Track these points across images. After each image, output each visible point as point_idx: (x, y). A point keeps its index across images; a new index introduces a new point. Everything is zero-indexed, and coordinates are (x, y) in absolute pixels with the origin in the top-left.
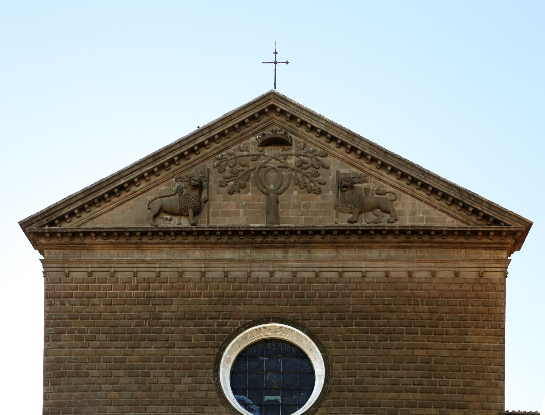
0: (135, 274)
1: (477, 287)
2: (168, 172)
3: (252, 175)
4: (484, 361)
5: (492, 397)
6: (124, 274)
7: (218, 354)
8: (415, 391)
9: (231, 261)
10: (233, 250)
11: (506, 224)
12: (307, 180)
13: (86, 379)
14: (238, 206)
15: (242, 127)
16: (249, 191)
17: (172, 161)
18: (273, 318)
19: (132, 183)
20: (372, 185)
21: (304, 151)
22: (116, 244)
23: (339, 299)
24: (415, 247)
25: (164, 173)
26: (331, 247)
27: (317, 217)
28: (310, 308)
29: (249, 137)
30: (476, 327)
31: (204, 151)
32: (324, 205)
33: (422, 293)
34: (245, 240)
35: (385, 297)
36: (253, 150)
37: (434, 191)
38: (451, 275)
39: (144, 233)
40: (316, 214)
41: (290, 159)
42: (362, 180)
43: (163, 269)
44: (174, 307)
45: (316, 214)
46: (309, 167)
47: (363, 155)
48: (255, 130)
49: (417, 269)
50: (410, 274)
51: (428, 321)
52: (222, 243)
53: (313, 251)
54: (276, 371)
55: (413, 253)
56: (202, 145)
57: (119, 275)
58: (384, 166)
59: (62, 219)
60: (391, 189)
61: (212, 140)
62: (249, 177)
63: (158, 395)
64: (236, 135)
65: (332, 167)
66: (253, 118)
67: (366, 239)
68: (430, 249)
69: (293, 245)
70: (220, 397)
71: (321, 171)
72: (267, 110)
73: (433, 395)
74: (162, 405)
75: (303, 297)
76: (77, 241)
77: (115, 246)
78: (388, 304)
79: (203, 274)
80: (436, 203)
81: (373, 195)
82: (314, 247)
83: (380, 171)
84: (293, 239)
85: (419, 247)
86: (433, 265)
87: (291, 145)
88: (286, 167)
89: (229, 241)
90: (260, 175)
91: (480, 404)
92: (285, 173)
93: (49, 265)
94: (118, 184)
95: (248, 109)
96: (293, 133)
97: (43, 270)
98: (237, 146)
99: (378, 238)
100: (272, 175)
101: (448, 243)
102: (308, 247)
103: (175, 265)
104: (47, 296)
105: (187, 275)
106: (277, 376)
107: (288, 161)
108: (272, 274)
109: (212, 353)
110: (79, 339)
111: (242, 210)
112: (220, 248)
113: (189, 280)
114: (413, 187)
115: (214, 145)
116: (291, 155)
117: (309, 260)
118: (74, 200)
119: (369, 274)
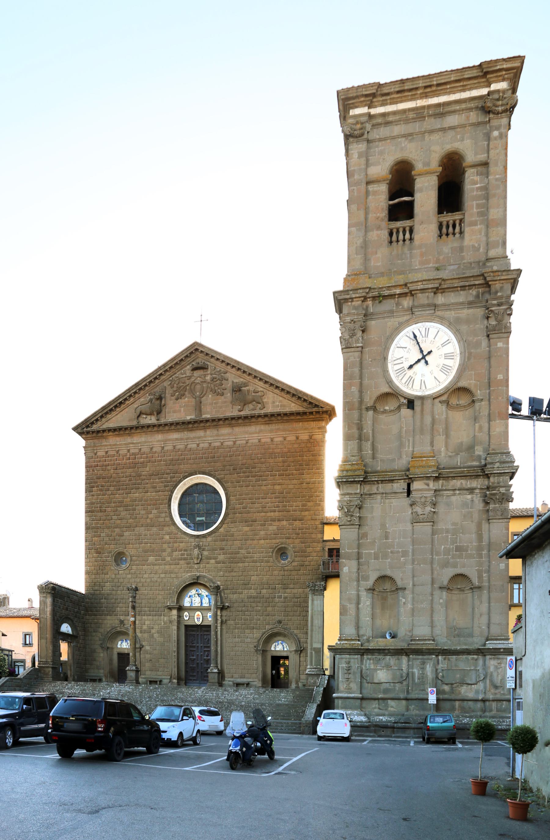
0: (129, 451)
1: (309, 445)
2: (144, 391)
3: (188, 388)
4: (313, 490)
5: (317, 512)
6: (123, 451)
7: (170, 495)
8: (275, 512)
9: (177, 439)
10: (178, 433)
11: (322, 407)
12: (216, 388)
13: (105, 513)
14: (181, 407)
15: (182, 362)
16: (186, 397)
17: (146, 386)
18: (199, 471)
19: (126, 400)
20: (251, 388)
21: (215, 371)
22: (119, 434)
23: (234, 458)
24: (274, 423)
25: (142, 392)
26: (229, 426)
27: (222, 409)
28: (218, 464)
29: (186, 366)
30: (308, 470)
31: (162, 377)
32: (225, 402)
33: (278, 450)
34: (183, 427)
35: (258, 454)
36: (188, 373)
37: (283, 390)
38: (294, 438)
39: (132, 428)
40: (221, 407)
41: (207, 377)
42: (246, 385)
43: (142, 447)
44: (148, 469)
45: (221, 407)
46: (217, 381)
47: (244, 372)
48: (189, 362)
49: (276, 436)
50: (272, 440)
51: (282, 468)
52: (172, 430)
53: (220, 429)
54: (202, 502)
55: (273, 427)
56: (161, 374)
57: (121, 452)
58: (255, 377)
59: (92, 423)
60: (262, 389)
61: (166, 371)
62: (186, 389)
63: (140, 521)
64: (179, 366)
65: (229, 379)
66: (187, 357)
67: (247, 421)
68: (283, 424)
69: (209, 428)
70: (171, 521)
71: (224, 382)
72: (194, 351)
73: (285, 513)
74: (142, 527)
75: (215, 458)
76: (100, 435)
77: (118, 435)
78: (260, 459)
79: (163, 448)
80: (285, 396)
81: (251, 394)
82: (220, 427)
83: (255, 380)
84: (208, 424)
85: (276, 423)
86: (284, 433)
87: (207, 369)
88: (205, 382)
89: (175, 428)
90: (192, 387)
91: (310, 517)
92: (205, 385)
93: (86, 449)
94: (119, 401)
95: (183, 353)
96: (209, 362)
97: (84, 452)
98: (180, 372)
99: (253, 420)
100: (198, 387)
101: (292, 420)
102: (217, 428)
103: (148, 444)
104: (87, 467)
105: (154, 450)
106: (203, 505)
107: (206, 378)
108: (198, 445)
109: (167, 494)
110: (101, 490)
111: (182, 409)
112: (171, 432)
113: (156, 452)
114: (272, 388)
115: (168, 373)
116: (208, 374)
117: (218, 435)
118: (97, 413)
119: (250, 441)
